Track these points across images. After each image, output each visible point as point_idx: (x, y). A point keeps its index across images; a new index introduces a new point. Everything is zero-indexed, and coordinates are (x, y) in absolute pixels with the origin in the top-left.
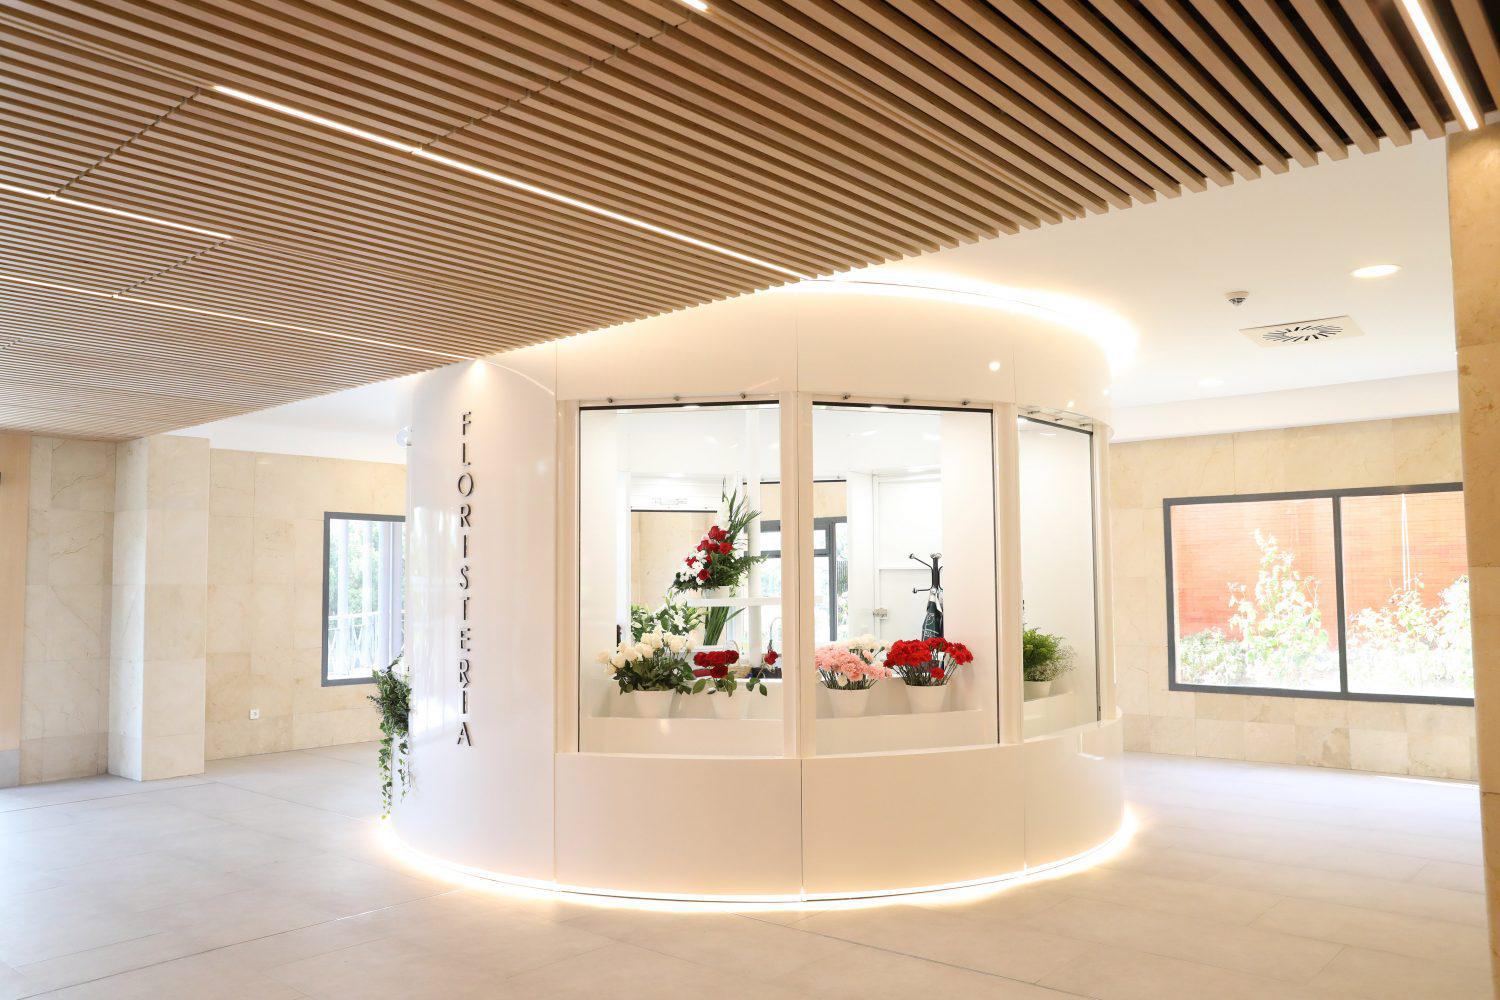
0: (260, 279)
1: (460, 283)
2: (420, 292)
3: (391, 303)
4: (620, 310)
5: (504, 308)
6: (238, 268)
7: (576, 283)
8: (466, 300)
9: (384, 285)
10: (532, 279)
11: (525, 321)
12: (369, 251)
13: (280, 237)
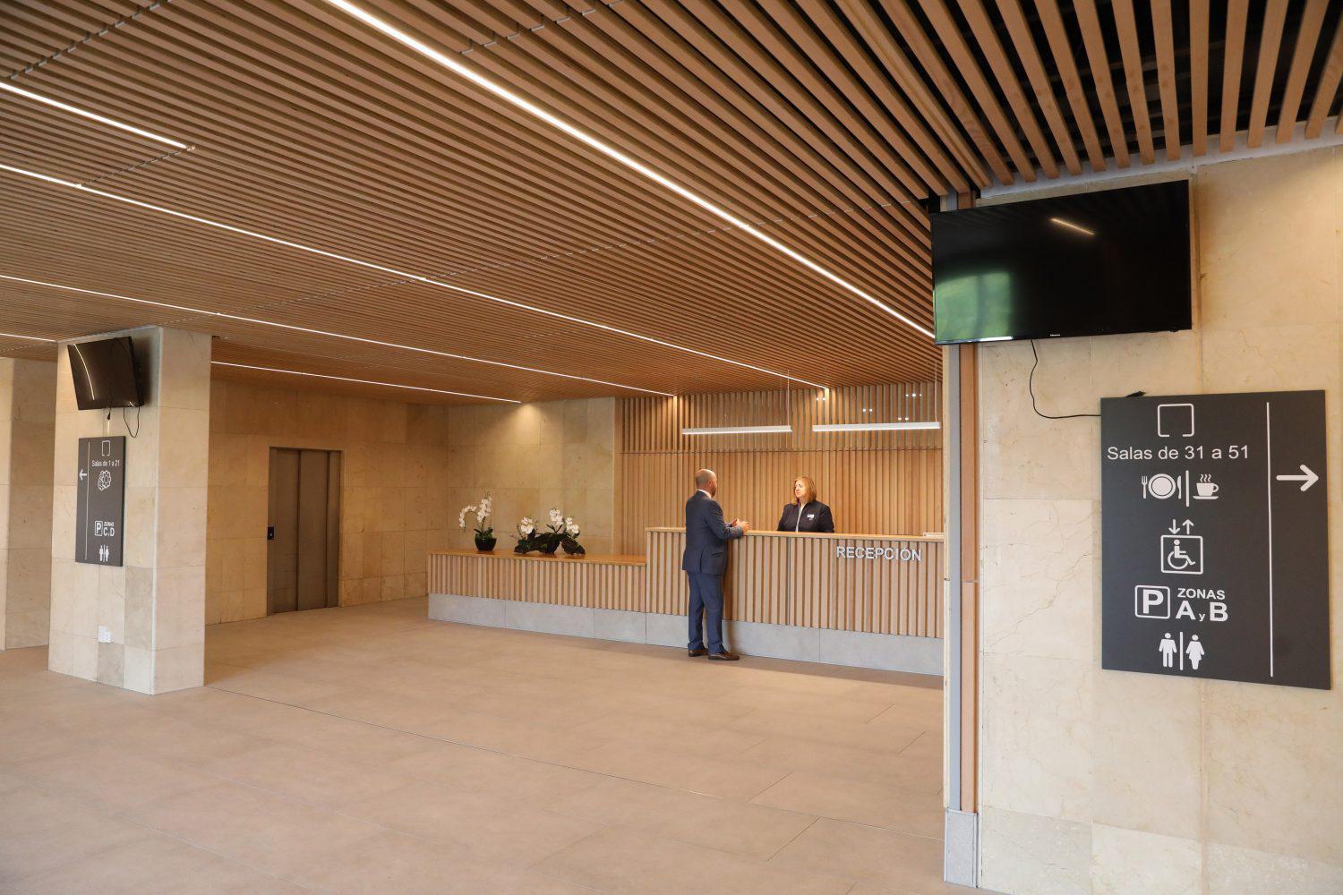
2: (394, 230)
3: (401, 232)
4: (329, 219)
5: (597, 268)
6: (666, 281)
8: (146, 183)
9: (609, 262)
10: (858, 316)
11: (645, 276)
12: (279, 155)
13: (365, 224)
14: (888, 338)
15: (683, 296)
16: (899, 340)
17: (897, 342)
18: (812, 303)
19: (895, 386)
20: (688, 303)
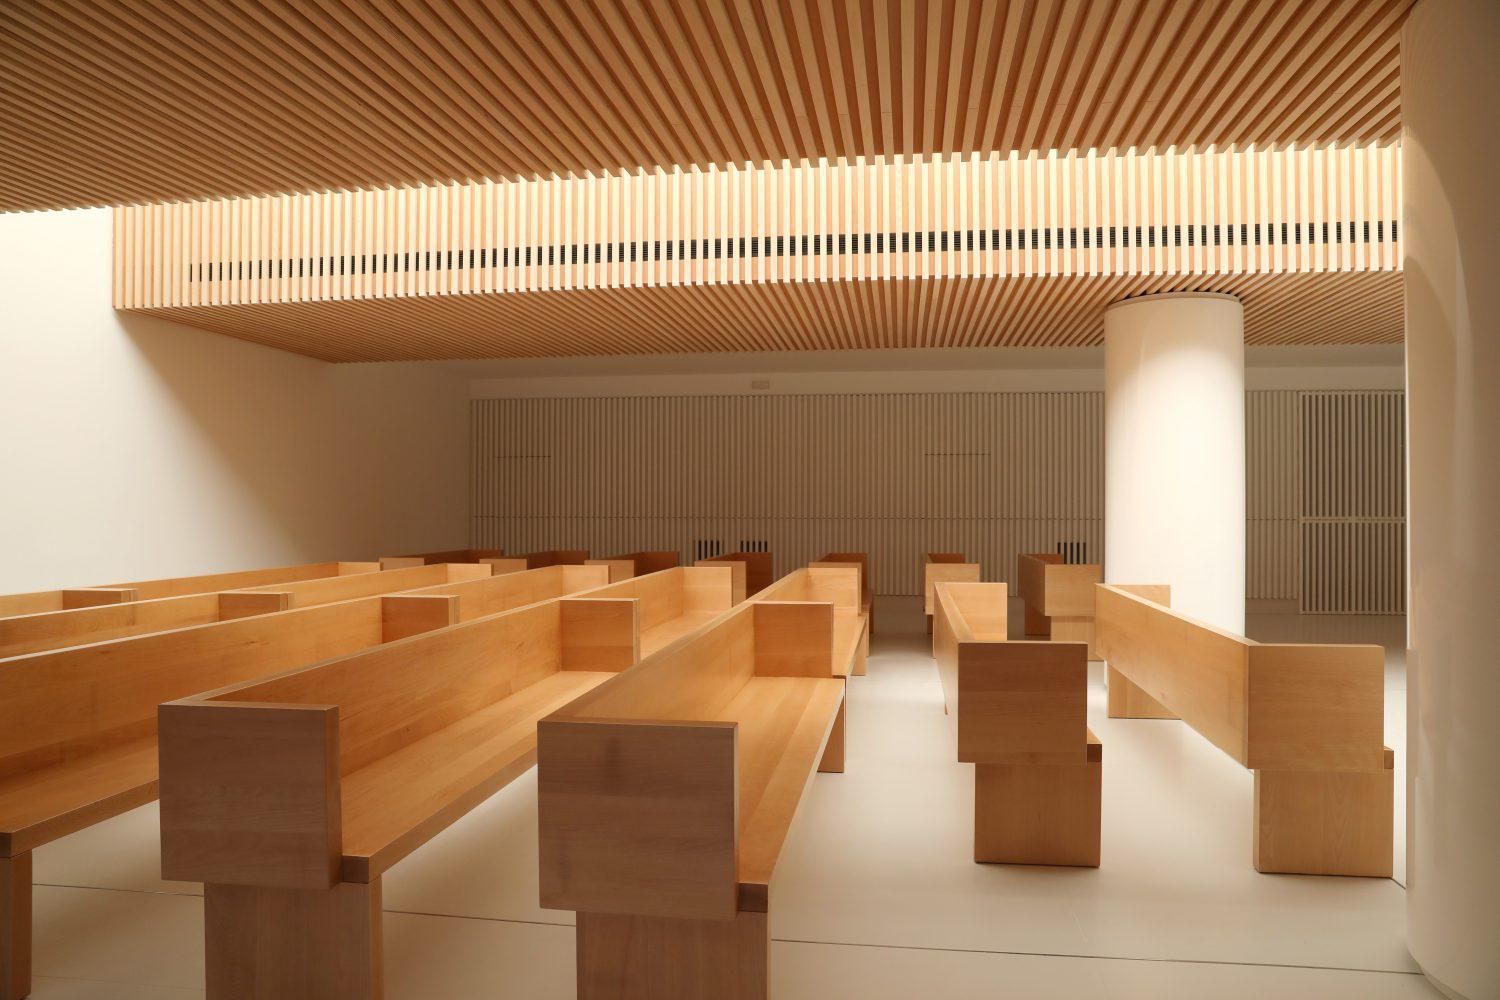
7: (1292, 312)
13: (111, 182)
14: (75, 192)
15: (1298, 303)
16: (27, 190)
17: (14, 146)
19: (345, 298)
20: (1269, 485)
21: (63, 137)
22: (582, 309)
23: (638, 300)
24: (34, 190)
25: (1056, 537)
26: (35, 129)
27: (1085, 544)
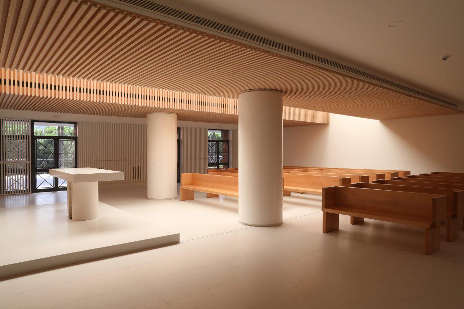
0: (268, 65)
1: (269, 64)
3: (266, 60)
7: (287, 67)
8: (193, 80)
9: (239, 72)
11: (181, 64)
12: (257, 62)
18: (155, 79)
21: (245, 73)
22: (270, 68)
23: (190, 81)
24: (244, 75)
25: (133, 165)
26: (164, 81)
27: (134, 179)
